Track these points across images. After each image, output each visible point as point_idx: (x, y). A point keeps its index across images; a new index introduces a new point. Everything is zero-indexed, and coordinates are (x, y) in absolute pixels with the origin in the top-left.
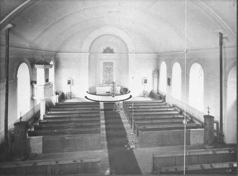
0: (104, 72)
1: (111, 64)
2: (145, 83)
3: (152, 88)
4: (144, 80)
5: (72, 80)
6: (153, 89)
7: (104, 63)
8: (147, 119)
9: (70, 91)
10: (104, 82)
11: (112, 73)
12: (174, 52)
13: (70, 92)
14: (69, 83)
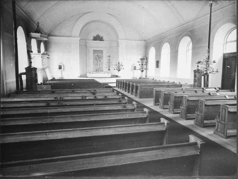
0: (94, 60)
1: (101, 52)
2: (134, 69)
3: (141, 75)
4: (133, 66)
5: (63, 66)
6: (142, 76)
7: (94, 50)
8: (26, 14)
9: (62, 76)
10: (95, 70)
11: (102, 61)
12: (165, 33)
13: (61, 77)
14: (60, 68)
